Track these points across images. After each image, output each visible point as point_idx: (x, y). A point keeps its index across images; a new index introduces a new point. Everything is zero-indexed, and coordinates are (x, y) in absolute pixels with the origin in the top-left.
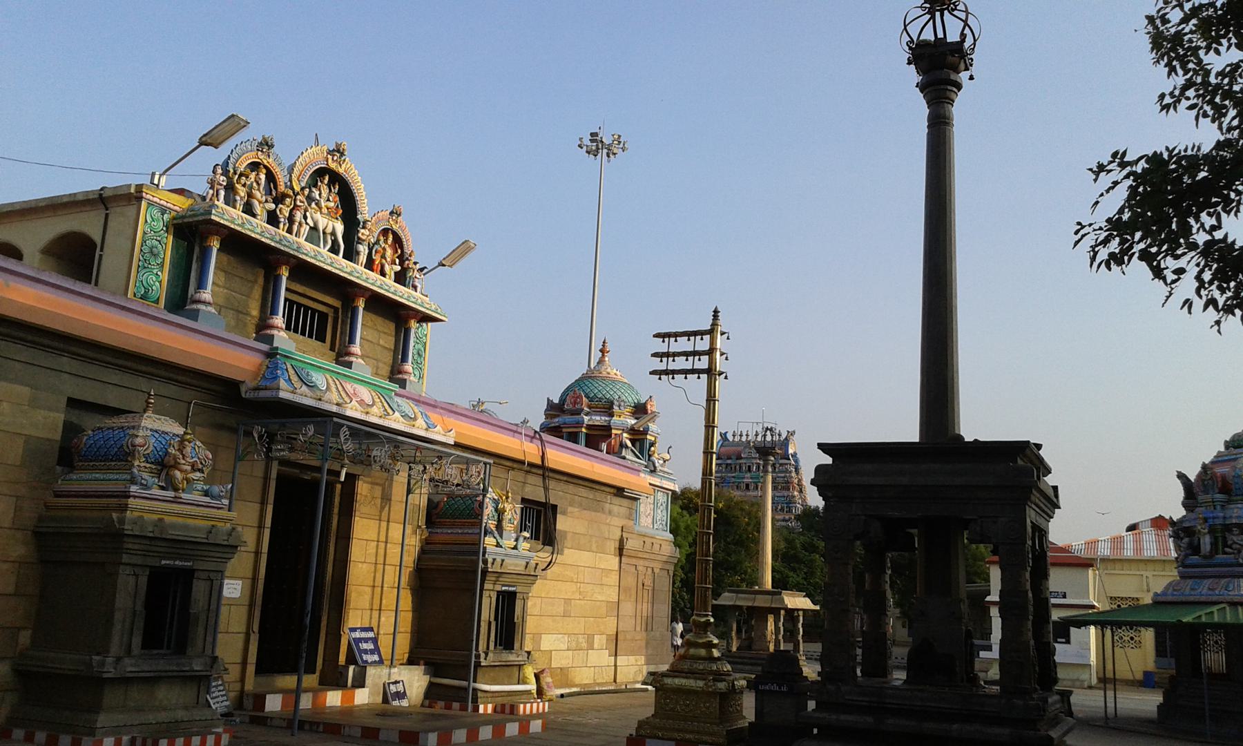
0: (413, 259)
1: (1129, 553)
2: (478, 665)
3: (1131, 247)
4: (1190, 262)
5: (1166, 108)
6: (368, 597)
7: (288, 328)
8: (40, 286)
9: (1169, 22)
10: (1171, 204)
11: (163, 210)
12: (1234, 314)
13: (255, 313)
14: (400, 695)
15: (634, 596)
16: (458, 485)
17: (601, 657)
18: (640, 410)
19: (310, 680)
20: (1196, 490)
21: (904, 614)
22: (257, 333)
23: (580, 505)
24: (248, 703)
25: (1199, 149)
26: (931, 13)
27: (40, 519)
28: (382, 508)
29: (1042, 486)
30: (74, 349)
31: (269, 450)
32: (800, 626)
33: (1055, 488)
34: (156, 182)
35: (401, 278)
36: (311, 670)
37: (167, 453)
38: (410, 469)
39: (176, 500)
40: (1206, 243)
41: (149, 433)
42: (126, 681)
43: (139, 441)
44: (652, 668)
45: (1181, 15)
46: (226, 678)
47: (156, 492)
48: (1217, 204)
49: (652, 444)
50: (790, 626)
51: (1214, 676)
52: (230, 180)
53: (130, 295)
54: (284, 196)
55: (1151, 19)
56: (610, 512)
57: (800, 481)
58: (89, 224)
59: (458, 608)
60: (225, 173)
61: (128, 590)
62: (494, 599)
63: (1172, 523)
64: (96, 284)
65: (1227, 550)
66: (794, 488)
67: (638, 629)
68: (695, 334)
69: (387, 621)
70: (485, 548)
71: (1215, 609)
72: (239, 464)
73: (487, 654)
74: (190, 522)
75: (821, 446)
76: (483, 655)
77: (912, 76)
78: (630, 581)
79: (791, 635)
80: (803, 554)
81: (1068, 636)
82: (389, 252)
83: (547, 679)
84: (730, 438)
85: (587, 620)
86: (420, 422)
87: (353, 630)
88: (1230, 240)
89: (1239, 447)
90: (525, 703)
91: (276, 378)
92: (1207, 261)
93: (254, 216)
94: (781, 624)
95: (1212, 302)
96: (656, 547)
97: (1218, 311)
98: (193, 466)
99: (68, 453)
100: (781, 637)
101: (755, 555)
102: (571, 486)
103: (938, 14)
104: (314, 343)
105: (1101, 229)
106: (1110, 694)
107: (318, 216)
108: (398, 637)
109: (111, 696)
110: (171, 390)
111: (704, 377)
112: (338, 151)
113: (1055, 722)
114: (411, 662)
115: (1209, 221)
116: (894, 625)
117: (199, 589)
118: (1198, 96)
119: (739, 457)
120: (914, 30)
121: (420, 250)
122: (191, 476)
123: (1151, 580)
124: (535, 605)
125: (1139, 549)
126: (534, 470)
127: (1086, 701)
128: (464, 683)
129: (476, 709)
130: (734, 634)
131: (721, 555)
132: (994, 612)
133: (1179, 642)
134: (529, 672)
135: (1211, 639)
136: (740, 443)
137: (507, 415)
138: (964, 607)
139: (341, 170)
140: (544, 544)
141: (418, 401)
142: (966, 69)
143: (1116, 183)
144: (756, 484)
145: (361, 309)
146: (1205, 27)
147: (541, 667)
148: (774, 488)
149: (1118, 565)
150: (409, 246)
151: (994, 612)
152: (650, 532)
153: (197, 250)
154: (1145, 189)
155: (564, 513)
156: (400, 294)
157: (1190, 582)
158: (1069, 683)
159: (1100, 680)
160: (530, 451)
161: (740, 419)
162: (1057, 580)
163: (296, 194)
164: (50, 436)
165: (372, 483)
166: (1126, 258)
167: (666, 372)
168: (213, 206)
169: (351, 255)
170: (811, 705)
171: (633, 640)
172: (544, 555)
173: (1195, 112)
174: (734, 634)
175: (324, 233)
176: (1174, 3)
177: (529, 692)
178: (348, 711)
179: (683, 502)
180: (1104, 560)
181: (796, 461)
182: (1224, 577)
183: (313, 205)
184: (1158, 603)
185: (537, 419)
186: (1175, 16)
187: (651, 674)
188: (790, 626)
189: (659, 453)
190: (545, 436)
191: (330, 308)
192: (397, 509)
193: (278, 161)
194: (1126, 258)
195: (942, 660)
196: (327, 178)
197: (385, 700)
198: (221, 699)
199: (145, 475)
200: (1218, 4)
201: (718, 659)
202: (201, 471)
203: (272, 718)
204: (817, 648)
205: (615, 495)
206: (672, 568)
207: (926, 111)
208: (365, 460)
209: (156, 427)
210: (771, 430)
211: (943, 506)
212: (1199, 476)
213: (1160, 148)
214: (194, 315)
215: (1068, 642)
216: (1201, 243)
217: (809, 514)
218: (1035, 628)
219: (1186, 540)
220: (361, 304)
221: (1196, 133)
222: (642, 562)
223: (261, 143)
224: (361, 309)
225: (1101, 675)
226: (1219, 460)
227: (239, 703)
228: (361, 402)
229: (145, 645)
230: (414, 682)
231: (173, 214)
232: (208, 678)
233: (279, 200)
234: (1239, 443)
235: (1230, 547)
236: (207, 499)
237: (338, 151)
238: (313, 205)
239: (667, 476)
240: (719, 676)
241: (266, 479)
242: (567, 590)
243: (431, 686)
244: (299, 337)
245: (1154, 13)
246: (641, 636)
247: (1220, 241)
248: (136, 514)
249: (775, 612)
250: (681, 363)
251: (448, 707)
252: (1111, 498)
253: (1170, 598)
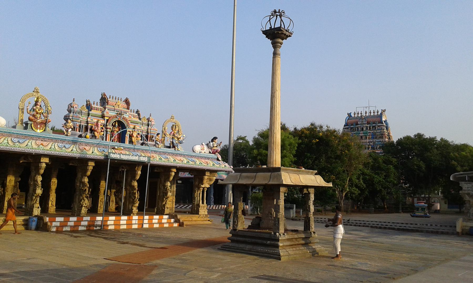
57: (389, 133)
66: (385, 137)
84: (353, 115)
119: (357, 124)
181: (387, 124)
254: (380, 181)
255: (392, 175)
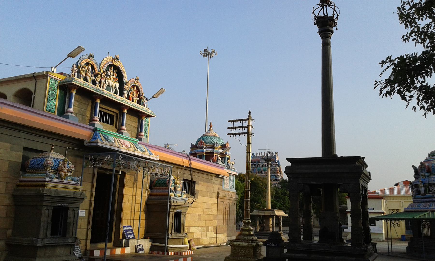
0: (143, 95)
1: (395, 193)
2: (168, 238)
3: (394, 89)
4: (415, 93)
5: (405, 40)
6: (129, 215)
7: (100, 121)
8: (13, 108)
9: (405, 9)
10: (408, 74)
11: (56, 80)
12: (431, 111)
13: (89, 115)
14: (141, 249)
15: (222, 213)
16: (161, 175)
17: (211, 234)
18: (224, 147)
19: (110, 245)
20: (419, 171)
21: (317, 216)
22: (89, 123)
23: (204, 181)
24: (88, 254)
25: (417, 54)
26: (322, 6)
27: (15, 190)
28: (134, 183)
29: (365, 172)
30: (26, 130)
31: (94, 164)
32: (281, 222)
33: (369, 173)
34: (53, 70)
35: (139, 102)
36: (110, 241)
37: (59, 166)
38: (144, 169)
39: (62, 183)
40: (420, 87)
41: (52, 159)
42: (45, 247)
43: (49, 162)
44: (230, 238)
45: (409, 7)
46: (80, 245)
47: (55, 180)
48: (424, 73)
49: (228, 159)
50: (277, 221)
51: (426, 237)
52: (79, 69)
53: (45, 110)
54: (98, 74)
55: (399, 9)
56: (214, 183)
57: (280, 170)
58: (30, 85)
59: (161, 219)
60: (77, 67)
61: (46, 215)
62: (174, 215)
63: (411, 183)
64: (33, 107)
65: (430, 192)
66: (278, 172)
67: (224, 224)
68: (243, 120)
69: (136, 223)
70: (170, 197)
71: (426, 213)
72: (84, 169)
73: (171, 234)
74: (67, 190)
75: (288, 160)
76: (170, 235)
77: (316, 29)
78: (221, 207)
79: (278, 225)
80: (282, 196)
81: (375, 223)
82: (135, 93)
83: (193, 243)
84: (256, 155)
85: (206, 220)
86: (147, 153)
87: (124, 227)
88: (428, 85)
89: (434, 156)
90: (185, 251)
91: (96, 138)
92: (420, 93)
93: (87, 81)
94: (274, 221)
95: (423, 107)
96: (230, 195)
97: (425, 110)
98: (68, 170)
99: (24, 167)
100: (274, 226)
101: (265, 196)
102: (200, 174)
103: (325, 7)
104: (109, 125)
105: (383, 83)
106: (390, 243)
107: (110, 81)
108: (140, 229)
109: (40, 252)
110: (60, 143)
111: (246, 135)
112: (116, 58)
113: (371, 255)
114: (145, 237)
115: (421, 79)
116: (314, 221)
117: (70, 214)
118: (416, 35)
119: (259, 162)
120: (316, 13)
121: (146, 92)
122: (67, 174)
123: (403, 203)
124: (188, 216)
125: (399, 192)
126: (187, 169)
127: (382, 246)
128: (164, 245)
129: (168, 254)
130: (258, 225)
131: (253, 197)
132: (349, 215)
133: (413, 225)
134: (186, 240)
135: (425, 223)
136: (259, 157)
137: (179, 150)
138: (338, 215)
139: (117, 65)
140: (191, 195)
141: (146, 145)
142: (335, 26)
143: (388, 67)
144: (265, 171)
145: (126, 113)
146: (418, 11)
147: (190, 238)
148: (271, 173)
149: (392, 198)
150: (142, 91)
151: (349, 215)
152: (228, 190)
153: (68, 94)
154: (398, 69)
155: (198, 184)
156: (139, 108)
157: (417, 204)
158: (376, 240)
159: (386, 238)
160: (186, 162)
161: (259, 148)
162: (371, 203)
163: (102, 74)
164: (17, 161)
165: (131, 175)
166: (392, 93)
167: (233, 134)
168: (73, 78)
169: (122, 94)
170: (285, 251)
171: (222, 228)
172: (191, 199)
173: (415, 41)
174: (258, 225)
175: (112, 87)
176: (407, 3)
177: (186, 247)
178: (123, 256)
179: (240, 178)
180: (387, 196)
181: (279, 163)
182: (429, 202)
183: (108, 77)
184: (406, 212)
185: (188, 151)
186: (407, 7)
187: (229, 241)
188: (277, 221)
189: (231, 162)
190: (191, 157)
191: (114, 114)
192: (139, 184)
193: (95, 62)
194: (392, 93)
195: (331, 234)
196: (113, 68)
197: (136, 251)
198: (78, 252)
199: (51, 174)
200: (422, 3)
201: (253, 235)
202: (71, 172)
203: (96, 259)
204: (287, 229)
205: (216, 177)
206: (236, 202)
207: (321, 41)
208: (128, 167)
209: (55, 157)
210: (270, 152)
211: (330, 179)
212: (419, 166)
213: (403, 54)
214: (67, 117)
215: (375, 225)
216: (418, 87)
217: (283, 182)
218: (363, 220)
219: (416, 189)
220: (126, 112)
221: (416, 49)
222: (225, 200)
223: (89, 56)
224: (126, 113)
225: (387, 237)
226: (426, 161)
227: (85, 253)
228: (126, 146)
229: (52, 234)
230: (146, 244)
231: (59, 81)
232: (74, 245)
233: (96, 76)
234: (434, 155)
235: (431, 191)
236: (73, 182)
237: (116, 58)
238: (108, 77)
239: (234, 170)
240: (253, 241)
241: (93, 174)
242: (199, 211)
243: (152, 246)
244: (104, 123)
245: (400, 6)
246: (225, 226)
247: (425, 86)
248: (48, 188)
249: (272, 217)
250: (238, 131)
251: (158, 253)
252: (389, 177)
253: (410, 210)
254: (280, 206)
255: (287, 202)
